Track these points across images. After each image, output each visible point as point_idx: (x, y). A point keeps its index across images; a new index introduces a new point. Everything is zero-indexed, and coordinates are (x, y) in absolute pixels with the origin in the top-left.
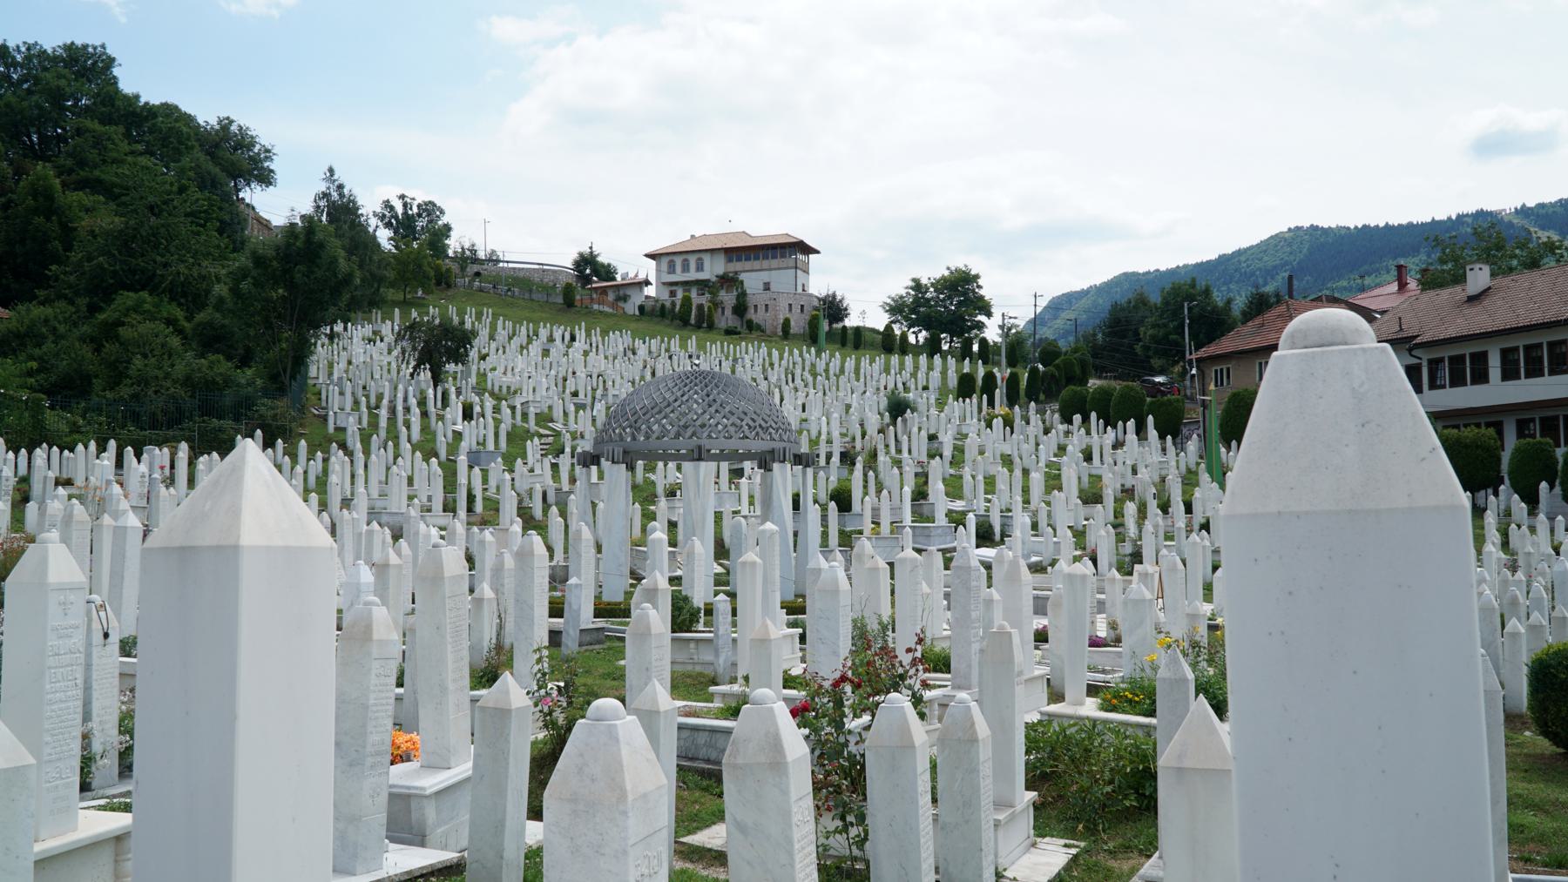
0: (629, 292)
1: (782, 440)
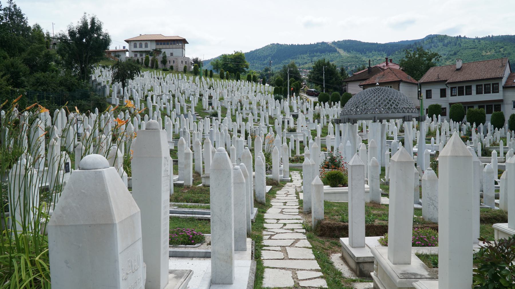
0: (120, 54)
1: (408, 112)
